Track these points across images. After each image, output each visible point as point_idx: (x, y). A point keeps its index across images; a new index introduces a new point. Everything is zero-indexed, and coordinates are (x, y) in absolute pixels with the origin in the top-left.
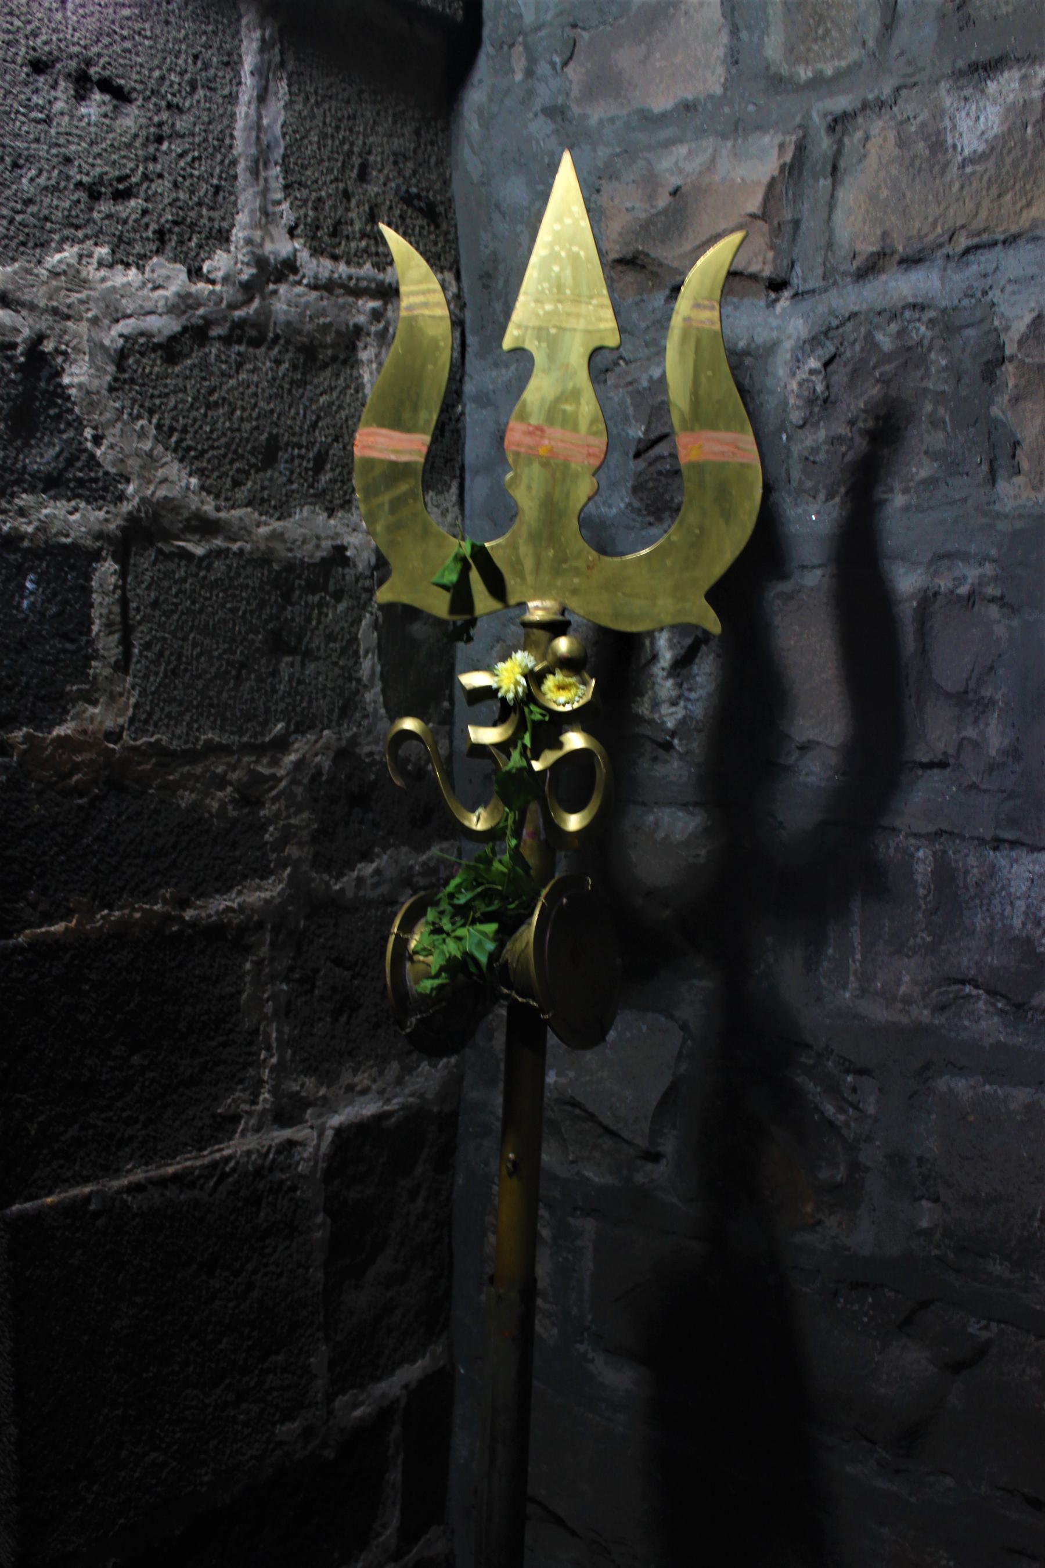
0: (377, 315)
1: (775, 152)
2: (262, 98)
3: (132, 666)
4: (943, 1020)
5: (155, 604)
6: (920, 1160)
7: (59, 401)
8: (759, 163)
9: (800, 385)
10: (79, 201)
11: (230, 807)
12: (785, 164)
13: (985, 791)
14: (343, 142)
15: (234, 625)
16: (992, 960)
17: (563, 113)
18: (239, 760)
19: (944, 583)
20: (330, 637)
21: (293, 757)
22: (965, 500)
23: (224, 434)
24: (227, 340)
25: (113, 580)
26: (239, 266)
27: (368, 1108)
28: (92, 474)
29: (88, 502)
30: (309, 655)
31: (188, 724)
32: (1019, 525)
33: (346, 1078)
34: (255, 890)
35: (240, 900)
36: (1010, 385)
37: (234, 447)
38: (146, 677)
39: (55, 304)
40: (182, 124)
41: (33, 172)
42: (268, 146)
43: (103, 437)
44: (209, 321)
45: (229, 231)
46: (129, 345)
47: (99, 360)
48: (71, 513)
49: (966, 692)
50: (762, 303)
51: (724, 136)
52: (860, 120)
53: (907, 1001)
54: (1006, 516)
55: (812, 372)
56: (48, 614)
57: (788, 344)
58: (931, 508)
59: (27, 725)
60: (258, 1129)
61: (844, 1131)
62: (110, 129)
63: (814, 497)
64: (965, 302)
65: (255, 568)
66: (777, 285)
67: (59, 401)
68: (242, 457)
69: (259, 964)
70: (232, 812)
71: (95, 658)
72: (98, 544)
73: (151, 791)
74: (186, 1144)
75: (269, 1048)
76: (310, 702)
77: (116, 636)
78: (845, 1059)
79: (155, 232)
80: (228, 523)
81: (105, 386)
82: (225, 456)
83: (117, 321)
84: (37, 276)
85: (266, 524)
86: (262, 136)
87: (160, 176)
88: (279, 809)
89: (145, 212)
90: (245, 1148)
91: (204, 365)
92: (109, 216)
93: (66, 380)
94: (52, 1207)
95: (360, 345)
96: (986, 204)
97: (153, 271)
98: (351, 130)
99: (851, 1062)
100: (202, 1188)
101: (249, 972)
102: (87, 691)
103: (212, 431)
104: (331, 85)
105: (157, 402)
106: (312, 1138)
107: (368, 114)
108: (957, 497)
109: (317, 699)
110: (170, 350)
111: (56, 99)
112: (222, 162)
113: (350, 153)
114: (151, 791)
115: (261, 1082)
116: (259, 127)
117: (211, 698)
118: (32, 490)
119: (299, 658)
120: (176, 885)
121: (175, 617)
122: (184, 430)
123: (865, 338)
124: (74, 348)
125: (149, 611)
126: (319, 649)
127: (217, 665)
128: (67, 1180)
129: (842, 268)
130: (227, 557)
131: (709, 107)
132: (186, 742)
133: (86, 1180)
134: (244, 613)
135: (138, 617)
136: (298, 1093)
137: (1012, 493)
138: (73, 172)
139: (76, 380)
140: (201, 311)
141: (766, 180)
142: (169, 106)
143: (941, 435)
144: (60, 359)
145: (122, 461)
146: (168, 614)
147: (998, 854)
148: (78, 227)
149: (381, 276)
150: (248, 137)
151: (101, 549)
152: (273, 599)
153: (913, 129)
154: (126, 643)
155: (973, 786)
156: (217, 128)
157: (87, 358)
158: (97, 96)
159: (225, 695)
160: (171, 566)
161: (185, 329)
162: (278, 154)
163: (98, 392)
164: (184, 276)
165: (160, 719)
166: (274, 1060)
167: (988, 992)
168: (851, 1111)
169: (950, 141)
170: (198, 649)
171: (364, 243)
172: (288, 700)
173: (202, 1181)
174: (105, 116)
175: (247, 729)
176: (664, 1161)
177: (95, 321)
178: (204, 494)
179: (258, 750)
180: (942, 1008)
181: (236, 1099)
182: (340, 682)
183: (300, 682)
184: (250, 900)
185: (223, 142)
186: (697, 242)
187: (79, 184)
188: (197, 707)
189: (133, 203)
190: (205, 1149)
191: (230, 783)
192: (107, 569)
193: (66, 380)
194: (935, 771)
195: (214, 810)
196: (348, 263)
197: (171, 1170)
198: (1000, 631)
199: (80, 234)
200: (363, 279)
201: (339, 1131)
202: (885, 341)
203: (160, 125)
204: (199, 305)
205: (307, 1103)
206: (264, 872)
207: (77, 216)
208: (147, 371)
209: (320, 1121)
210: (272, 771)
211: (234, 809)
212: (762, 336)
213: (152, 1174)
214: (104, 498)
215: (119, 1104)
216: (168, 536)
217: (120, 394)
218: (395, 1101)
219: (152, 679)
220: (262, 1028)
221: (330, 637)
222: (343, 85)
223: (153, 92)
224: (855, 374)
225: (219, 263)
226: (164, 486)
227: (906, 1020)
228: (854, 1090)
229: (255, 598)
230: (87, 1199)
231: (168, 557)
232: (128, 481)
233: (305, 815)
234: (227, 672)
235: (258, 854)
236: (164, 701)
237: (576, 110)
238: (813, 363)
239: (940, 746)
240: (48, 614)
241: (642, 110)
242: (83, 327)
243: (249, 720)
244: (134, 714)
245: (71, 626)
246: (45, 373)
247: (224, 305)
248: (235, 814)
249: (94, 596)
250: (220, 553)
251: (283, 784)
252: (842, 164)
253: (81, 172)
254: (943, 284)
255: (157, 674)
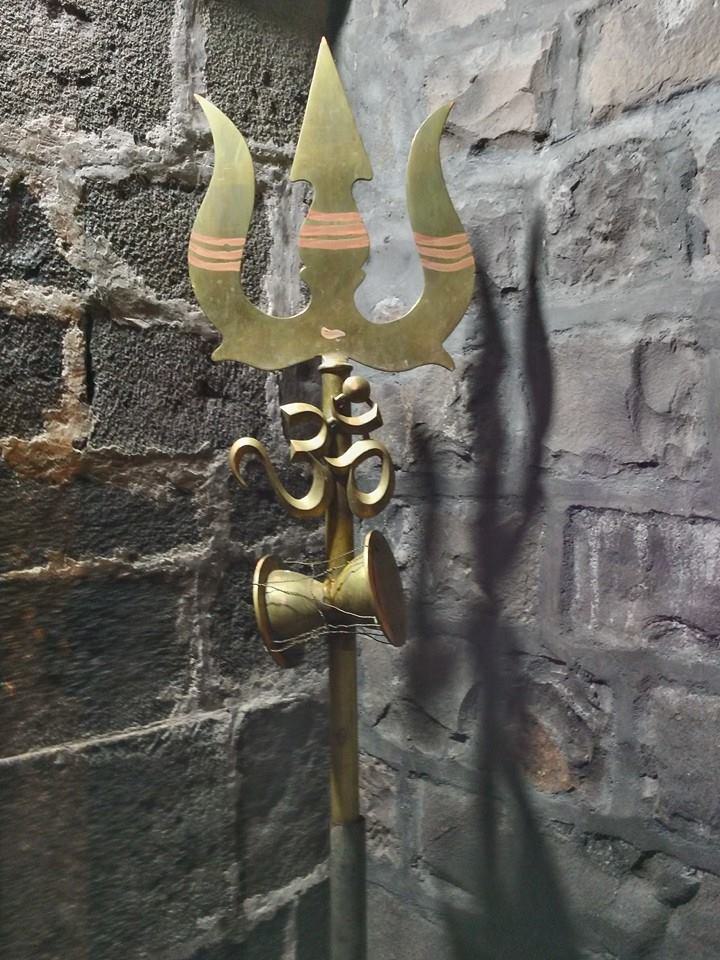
0: (277, 176)
1: (540, 44)
2: (190, 24)
3: (94, 399)
4: (657, 646)
5: (112, 359)
6: (643, 746)
7: (37, 219)
8: (532, 51)
9: (555, 204)
10: (50, 85)
11: (168, 495)
12: (546, 51)
13: (685, 482)
14: (252, 58)
15: (172, 375)
16: (693, 603)
17: (403, 35)
18: (175, 464)
19: (654, 335)
20: (244, 387)
21: (216, 464)
22: (669, 275)
23: (163, 249)
24: (166, 186)
25: (79, 340)
26: (173, 136)
27: (270, 699)
28: (63, 269)
29: (59, 288)
30: (227, 398)
31: (137, 439)
32: (707, 289)
33: (255, 678)
34: (187, 551)
35: (175, 556)
36: (702, 189)
37: (170, 257)
38: (104, 406)
39: (32, 153)
40: (129, 38)
41: (15, 64)
42: (195, 56)
43: (71, 245)
44: (150, 173)
45: (165, 113)
46: (89, 184)
47: (67, 192)
48: (46, 294)
49: (670, 412)
50: (531, 152)
51: (506, 38)
52: (597, 13)
53: (631, 632)
54: (699, 284)
55: (562, 195)
56: (29, 360)
57: (547, 178)
58: (646, 283)
59: (12, 434)
60: (187, 712)
61: (589, 724)
62: (74, 38)
63: (565, 283)
64: (670, 134)
65: (187, 339)
66: (541, 137)
67: (37, 219)
68: (177, 264)
69: (190, 600)
70: (170, 498)
71: (65, 392)
72: (67, 316)
73: (109, 482)
74: (132, 720)
75: (196, 657)
76: (229, 429)
77: (82, 378)
78: (589, 673)
79: (108, 109)
80: (165, 307)
81: (72, 210)
82: (164, 263)
83: (81, 167)
84: (19, 133)
85: (195, 310)
86: (190, 50)
87: (113, 72)
88: (206, 498)
89: (101, 96)
90: (177, 724)
91: (147, 201)
92: (73, 97)
93: (41, 205)
94: (26, 762)
95: (266, 195)
96: (684, 61)
97: (107, 135)
98: (258, 50)
99: (593, 676)
100: (143, 751)
101: (181, 605)
102: (59, 413)
103: (153, 246)
104: (243, 19)
105: (112, 224)
106: (226, 719)
107: (271, 40)
108: (664, 274)
109: (234, 427)
110: (122, 190)
111: (34, 16)
112: (160, 65)
113: (257, 66)
114: (109, 482)
115: (190, 679)
116: (188, 44)
117: (153, 422)
118: (16, 277)
119: (221, 400)
120: (127, 545)
121: (127, 368)
122: (133, 244)
123: (599, 167)
124: (47, 184)
125: (106, 363)
126: (235, 394)
127: (159, 401)
128: (36, 743)
129: (585, 119)
130: (166, 331)
131: (497, 19)
132: (135, 451)
133: (54, 743)
134: (179, 368)
135: (99, 367)
136: (218, 687)
137: (703, 267)
138: (46, 65)
139: (49, 205)
140: (144, 165)
141: (534, 62)
142: (120, 25)
143: (652, 231)
144: (37, 191)
145: (85, 261)
146: (122, 366)
147: (694, 526)
148: (50, 103)
149: (280, 149)
150: (179, 50)
151: (69, 319)
152: (201, 360)
153: (633, 15)
154: (89, 382)
155: (675, 478)
156: (156, 42)
157: (57, 191)
158: (65, 16)
159: (164, 421)
160: (123, 334)
161: (132, 177)
162: (202, 62)
163: (66, 215)
164: (131, 140)
165: (115, 435)
166: (200, 665)
167: (689, 626)
168: (593, 709)
169: (659, 21)
170: (144, 390)
171: (267, 127)
172: (213, 427)
173: (143, 746)
174: (71, 29)
175: (181, 445)
176: (468, 741)
177: (63, 166)
178: (148, 287)
179: (191, 459)
180: (657, 637)
181: (170, 690)
182: (251, 417)
183: (220, 416)
184: (183, 557)
185: (161, 52)
186: (488, 114)
187: (50, 74)
188: (143, 428)
189: (92, 88)
190: (146, 724)
191: (169, 480)
192: (74, 335)
193: (41, 205)
194: (649, 469)
195: (156, 497)
196: (256, 139)
197: (120, 737)
198: (694, 367)
199: (52, 107)
200: (266, 150)
201: (248, 714)
202: (613, 168)
203: (113, 38)
204: (143, 161)
205: (224, 695)
206: (193, 539)
207: (49, 95)
208: (103, 203)
209: (235, 707)
210: (200, 473)
211: (172, 497)
212: (530, 174)
213: (105, 740)
214: (72, 286)
215: (82, 691)
216: (121, 315)
217: (82, 216)
218: (291, 695)
219: (109, 408)
220: (191, 643)
221: (244, 387)
222: (252, 20)
223: (107, 15)
224: (593, 194)
225: (158, 133)
226: (117, 280)
227: (630, 646)
228: (596, 695)
229: (188, 358)
230: (53, 757)
231: (122, 328)
232: (90, 275)
233: (225, 502)
234: (166, 406)
235: (190, 527)
236: (118, 423)
237: (411, 32)
238: (564, 189)
239: (651, 451)
240: (29, 360)
241: (453, 27)
242: (54, 170)
243: (183, 438)
244: (95, 431)
245: (47, 370)
246: (26, 199)
247: (162, 162)
248: (172, 500)
249: (64, 351)
250: (160, 327)
251: (208, 482)
252: (585, 47)
253: (52, 66)
254: (654, 123)
255: (113, 405)
